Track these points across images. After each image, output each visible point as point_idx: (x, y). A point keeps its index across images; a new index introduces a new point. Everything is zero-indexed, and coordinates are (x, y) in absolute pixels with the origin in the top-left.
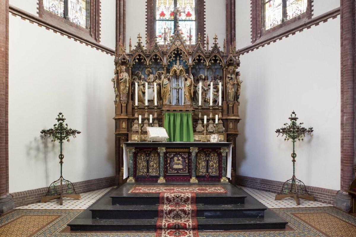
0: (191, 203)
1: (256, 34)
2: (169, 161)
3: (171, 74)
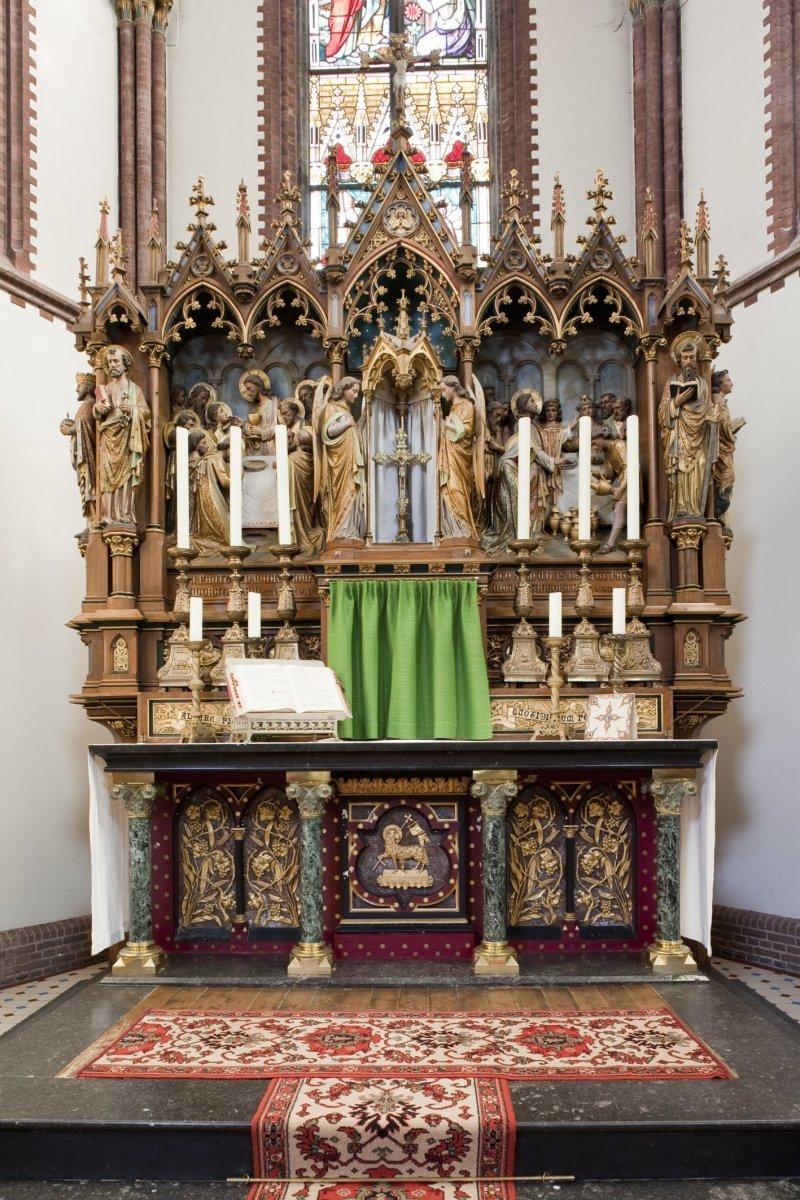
0: (484, 1169)
2: (352, 850)
3: (365, 385)
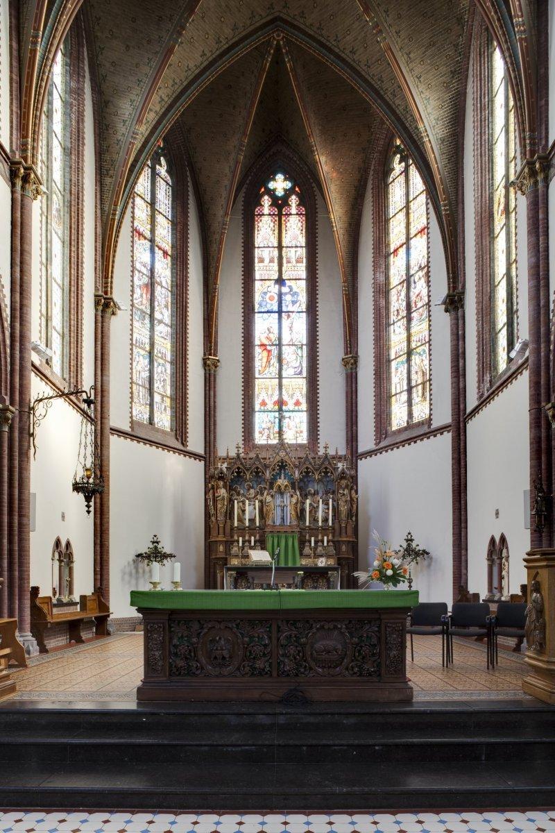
1: (381, 435)
